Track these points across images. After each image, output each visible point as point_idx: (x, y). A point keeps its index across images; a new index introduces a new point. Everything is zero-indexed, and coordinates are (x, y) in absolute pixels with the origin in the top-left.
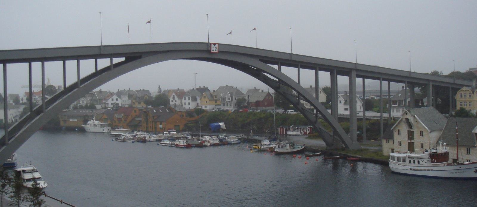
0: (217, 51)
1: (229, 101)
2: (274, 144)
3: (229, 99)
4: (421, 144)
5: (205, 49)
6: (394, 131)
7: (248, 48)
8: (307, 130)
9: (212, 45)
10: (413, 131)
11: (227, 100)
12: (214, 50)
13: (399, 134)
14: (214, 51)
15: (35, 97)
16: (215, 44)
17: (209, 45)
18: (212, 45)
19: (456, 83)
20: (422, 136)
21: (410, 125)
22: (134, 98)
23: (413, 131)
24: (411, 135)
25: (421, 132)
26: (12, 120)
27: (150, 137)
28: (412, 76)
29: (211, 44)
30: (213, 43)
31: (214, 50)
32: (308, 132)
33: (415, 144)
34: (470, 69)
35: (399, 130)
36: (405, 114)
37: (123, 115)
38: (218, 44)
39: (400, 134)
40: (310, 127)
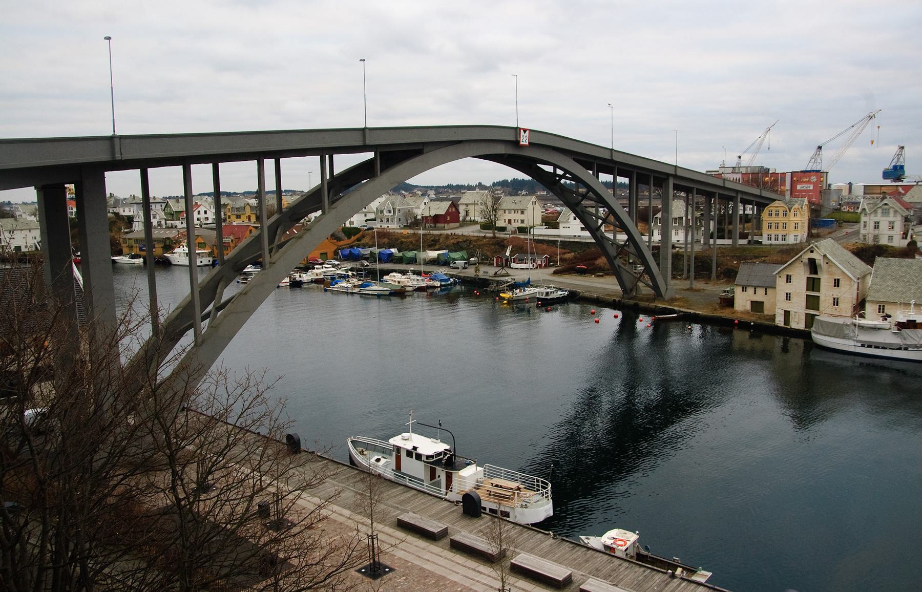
0: (527, 144)
1: (390, 215)
2: (530, 291)
3: (389, 212)
4: (834, 299)
5: (511, 137)
6: (777, 276)
7: (166, 139)
8: (542, 261)
9: (522, 131)
10: (820, 279)
11: (386, 213)
12: (524, 140)
13: (787, 282)
14: (524, 143)
15: (72, 209)
16: (525, 131)
17: (517, 130)
18: (522, 131)
19: (763, 195)
20: (838, 286)
21: (813, 266)
22: (229, 209)
23: (820, 279)
24: (813, 284)
25: (835, 280)
26: (36, 247)
27: (300, 276)
28: (727, 186)
29: (520, 129)
30: (522, 129)
31: (524, 140)
32: (543, 265)
33: (822, 299)
34: (707, 172)
35: (787, 276)
36: (809, 252)
37: (231, 237)
38: (530, 130)
39: (790, 282)
40: (546, 257)
